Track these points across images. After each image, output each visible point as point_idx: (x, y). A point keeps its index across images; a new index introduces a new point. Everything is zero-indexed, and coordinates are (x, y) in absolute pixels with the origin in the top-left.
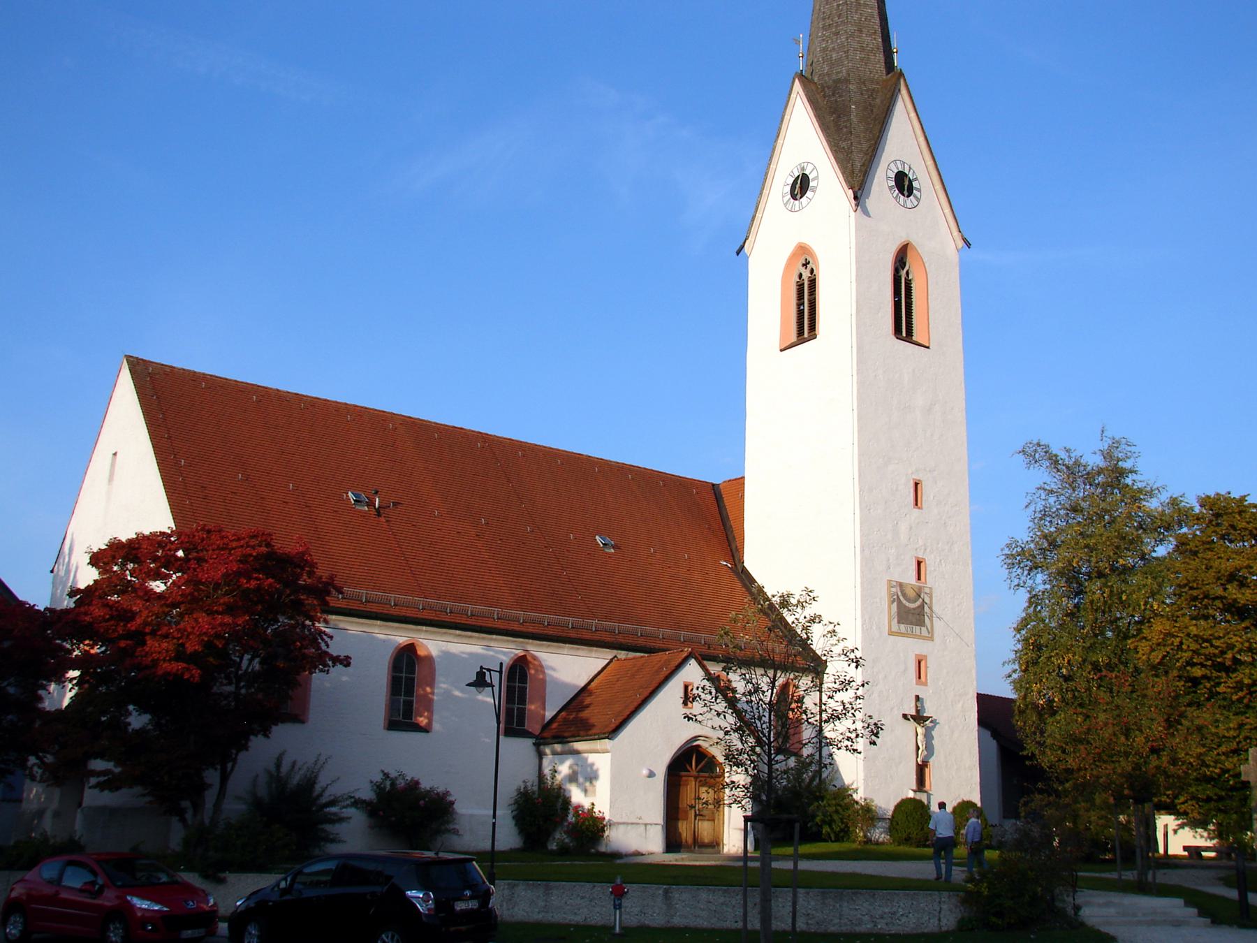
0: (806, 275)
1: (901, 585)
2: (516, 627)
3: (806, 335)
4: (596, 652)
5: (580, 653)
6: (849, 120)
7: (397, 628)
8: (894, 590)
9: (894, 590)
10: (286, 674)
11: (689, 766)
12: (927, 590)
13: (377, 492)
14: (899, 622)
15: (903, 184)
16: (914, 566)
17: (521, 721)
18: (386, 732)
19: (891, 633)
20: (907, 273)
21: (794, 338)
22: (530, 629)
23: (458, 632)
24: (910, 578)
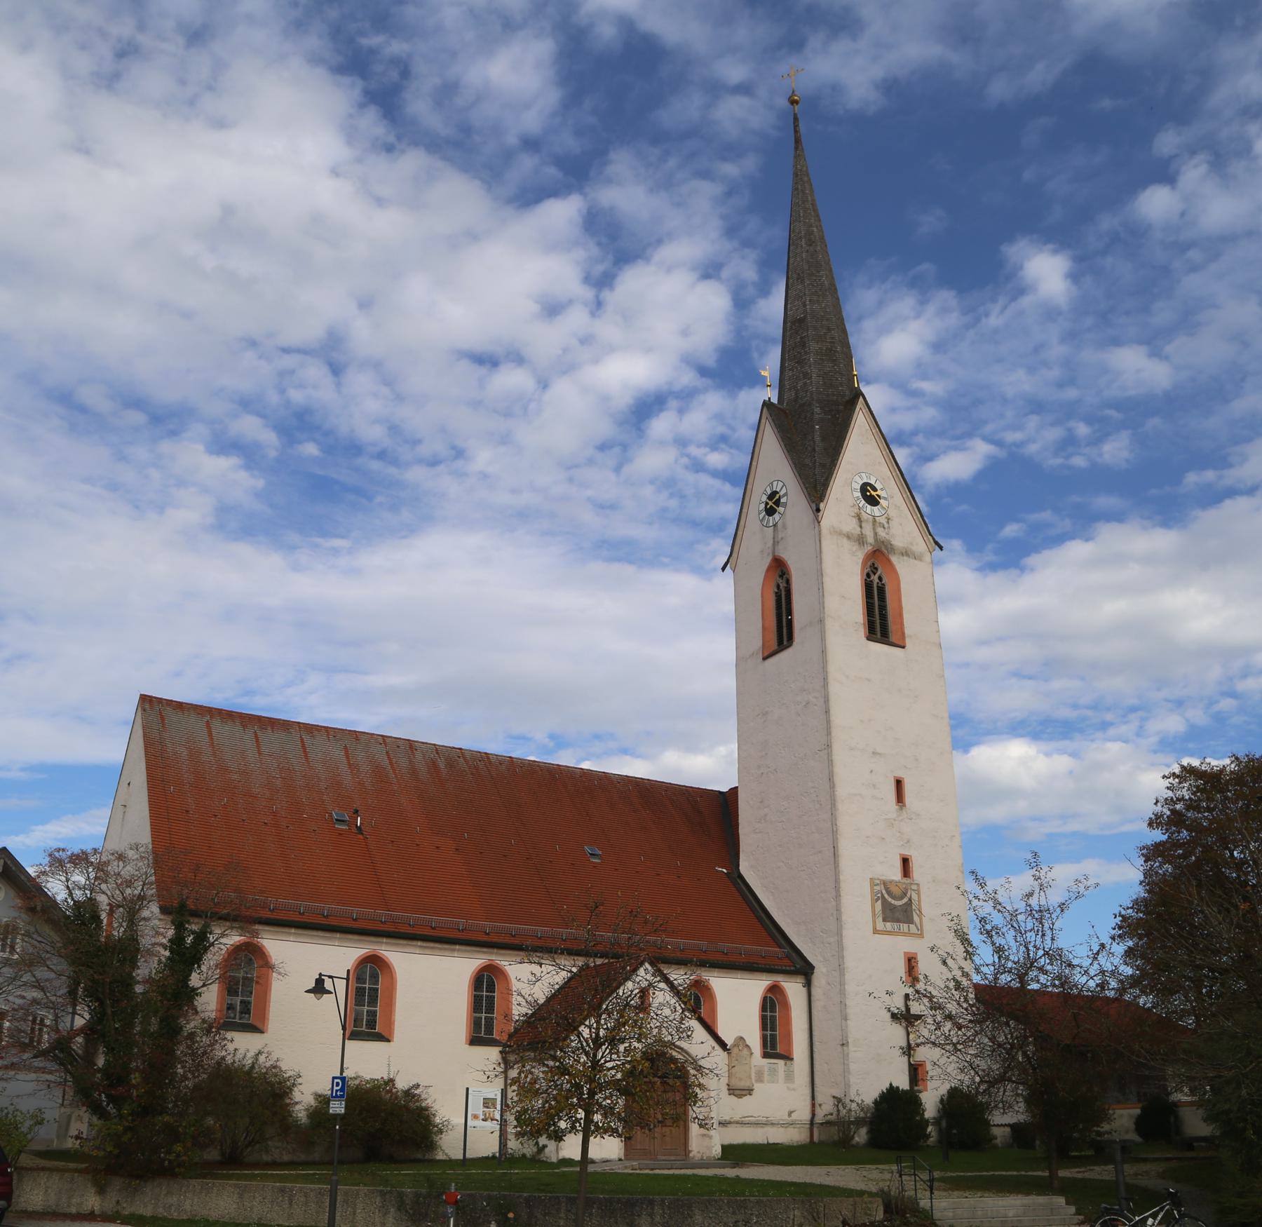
1: (884, 883)
2: (485, 938)
5: (454, 950)
8: (877, 888)
9: (877, 888)
12: (914, 887)
14: (884, 920)
15: (869, 496)
16: (898, 864)
17: (489, 1029)
19: (876, 931)
20: (880, 578)
21: (775, 647)
23: (419, 943)
24: (895, 874)
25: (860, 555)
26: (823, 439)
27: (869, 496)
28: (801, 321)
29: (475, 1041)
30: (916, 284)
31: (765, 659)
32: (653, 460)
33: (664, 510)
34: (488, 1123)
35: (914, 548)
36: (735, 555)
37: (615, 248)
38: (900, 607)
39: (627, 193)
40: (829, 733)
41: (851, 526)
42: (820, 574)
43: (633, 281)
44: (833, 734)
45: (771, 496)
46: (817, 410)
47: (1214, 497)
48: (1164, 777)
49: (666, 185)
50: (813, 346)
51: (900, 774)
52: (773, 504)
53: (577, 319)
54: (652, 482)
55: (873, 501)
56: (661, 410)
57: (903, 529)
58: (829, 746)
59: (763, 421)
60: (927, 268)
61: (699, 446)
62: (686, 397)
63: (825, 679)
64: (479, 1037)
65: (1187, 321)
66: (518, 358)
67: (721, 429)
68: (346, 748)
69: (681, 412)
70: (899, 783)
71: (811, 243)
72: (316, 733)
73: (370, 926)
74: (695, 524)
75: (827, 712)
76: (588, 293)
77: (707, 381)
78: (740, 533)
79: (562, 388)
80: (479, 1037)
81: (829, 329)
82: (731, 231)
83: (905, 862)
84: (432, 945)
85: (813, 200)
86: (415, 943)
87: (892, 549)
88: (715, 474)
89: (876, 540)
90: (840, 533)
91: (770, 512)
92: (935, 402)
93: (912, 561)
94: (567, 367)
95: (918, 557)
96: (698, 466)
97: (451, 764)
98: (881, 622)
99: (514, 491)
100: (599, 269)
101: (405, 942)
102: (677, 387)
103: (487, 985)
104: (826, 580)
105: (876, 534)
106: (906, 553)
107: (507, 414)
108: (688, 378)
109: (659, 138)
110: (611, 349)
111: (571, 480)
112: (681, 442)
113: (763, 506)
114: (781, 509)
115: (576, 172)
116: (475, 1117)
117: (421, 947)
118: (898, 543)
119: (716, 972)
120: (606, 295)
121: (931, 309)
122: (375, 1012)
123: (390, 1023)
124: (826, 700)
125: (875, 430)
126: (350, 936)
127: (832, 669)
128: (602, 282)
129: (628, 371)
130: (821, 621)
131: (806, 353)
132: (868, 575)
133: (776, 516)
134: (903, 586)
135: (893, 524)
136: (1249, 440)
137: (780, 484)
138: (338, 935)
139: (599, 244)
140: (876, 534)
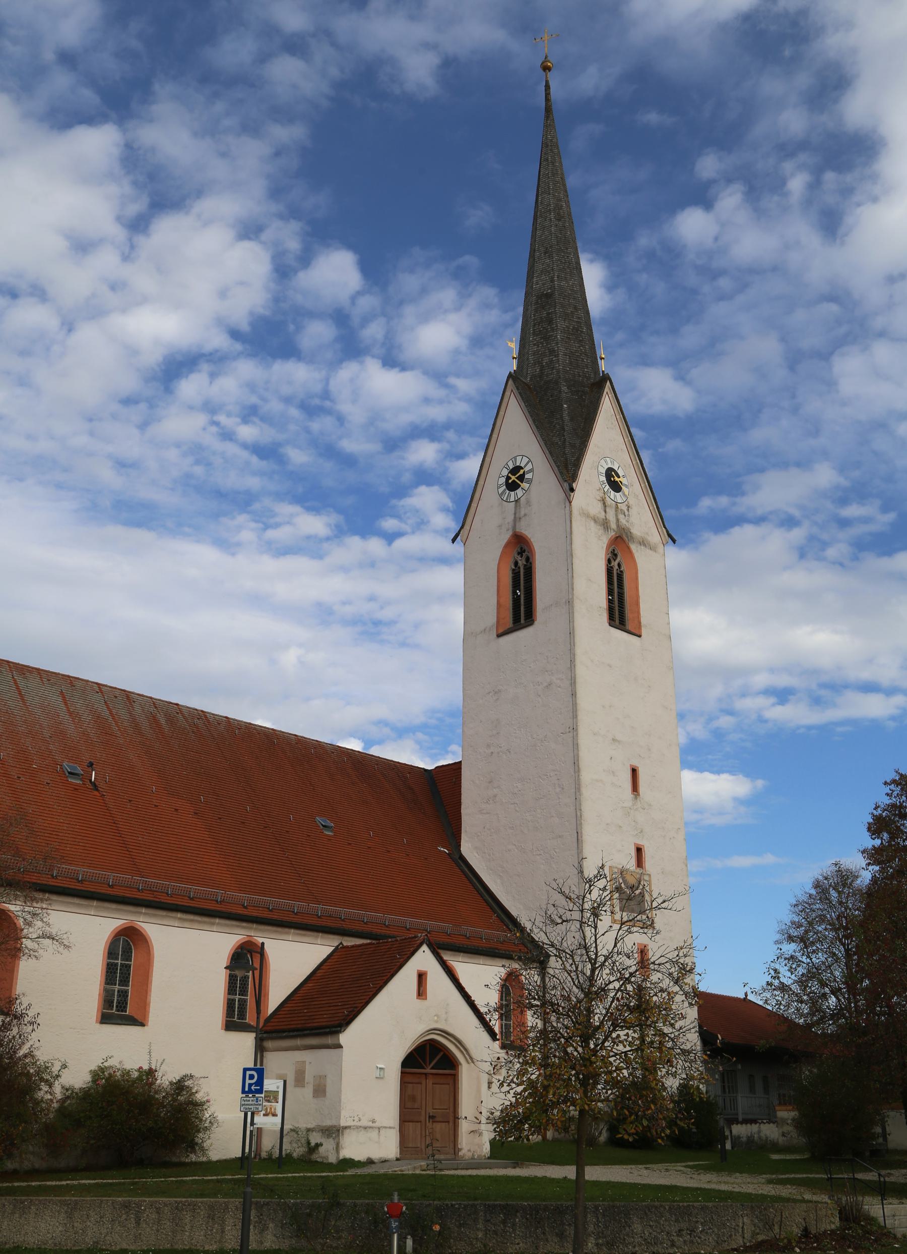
0: (522, 563)
2: (241, 911)
3: (522, 621)
4: (321, 938)
6: (562, 417)
7: (79, 905)
10: (446, 377)
11: (430, 1063)
13: (91, 765)
15: (613, 481)
16: (633, 853)
18: (98, 1025)
20: (619, 565)
21: (509, 623)
22: (255, 914)
23: (179, 915)
24: (631, 865)
25: (605, 541)
26: (572, 420)
27: (613, 481)
28: (549, 296)
29: (231, 1025)
30: (459, 275)
31: (499, 636)
32: (181, 424)
33: (188, 476)
35: (650, 539)
36: (467, 527)
37: (157, 194)
39: (170, 134)
40: (575, 716)
41: (596, 509)
42: (570, 555)
43: (167, 230)
44: (579, 718)
45: (515, 470)
46: (564, 389)
47: (724, 523)
48: (886, 783)
49: (209, 130)
50: (561, 324)
51: (635, 763)
52: (515, 479)
53: (107, 261)
54: (178, 445)
55: (616, 487)
56: (191, 371)
57: (641, 520)
58: (574, 729)
59: (508, 393)
60: (471, 260)
61: (229, 415)
62: (216, 361)
63: (572, 662)
64: (234, 1021)
65: (712, 348)
66: (39, 293)
67: (254, 399)
69: (213, 376)
70: (634, 771)
71: (559, 218)
73: (128, 894)
74: (220, 494)
75: (574, 694)
76: (118, 233)
77: (238, 347)
78: (474, 505)
79: (88, 335)
80: (234, 1021)
81: (575, 308)
82: (276, 192)
83: (639, 850)
84: (191, 917)
85: (562, 174)
86: (174, 914)
87: (631, 536)
88: (245, 446)
89: (618, 526)
90: (587, 516)
91: (512, 486)
92: (468, 399)
93: (648, 551)
94: (94, 311)
95: (653, 548)
96: (227, 436)
97: (171, 720)
98: (620, 612)
99: (30, 437)
100: (134, 209)
101: (164, 913)
102: (209, 347)
103: (246, 964)
104: (576, 561)
105: (618, 520)
106: (643, 543)
107: (24, 353)
108: (219, 341)
109: (214, 82)
110: (143, 300)
111: (92, 434)
112: (210, 408)
113: (503, 480)
114: (525, 485)
115: (118, 102)
117: (180, 919)
118: (636, 531)
119: (461, 957)
120: (140, 240)
121: (472, 302)
122: (126, 992)
123: (144, 1005)
124: (573, 682)
125: (619, 416)
126: (107, 905)
127: (579, 651)
128: (138, 225)
129: (156, 327)
130: (570, 603)
131: (553, 330)
132: (609, 561)
133: (519, 492)
134: (640, 575)
135: (633, 511)
136: (762, 470)
137: (525, 460)
138: (95, 903)
139: (135, 183)
140: (618, 520)
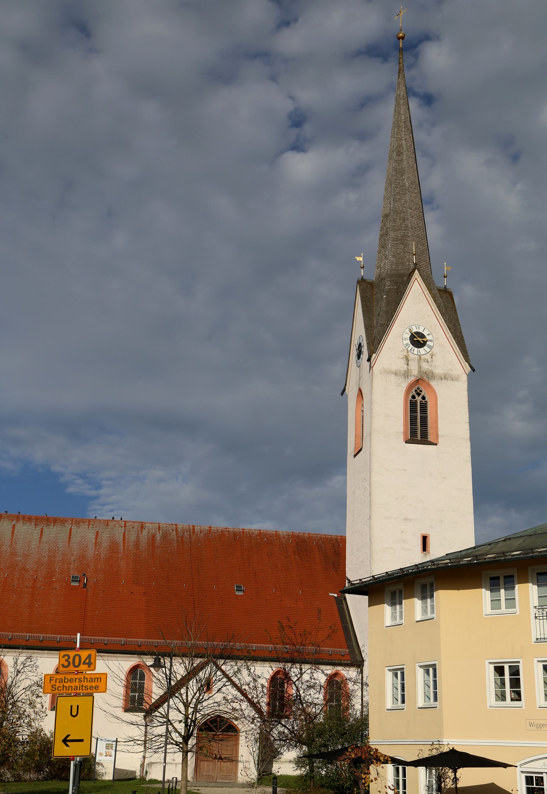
20: (424, 398)
25: (405, 385)
27: (418, 340)
34: (108, 757)
38: (437, 416)
41: (401, 366)
68: (97, 532)
70: (425, 539)
72: (82, 524)
89: (420, 372)
93: (449, 382)
116: (101, 754)
117: (47, 653)
118: (438, 371)
